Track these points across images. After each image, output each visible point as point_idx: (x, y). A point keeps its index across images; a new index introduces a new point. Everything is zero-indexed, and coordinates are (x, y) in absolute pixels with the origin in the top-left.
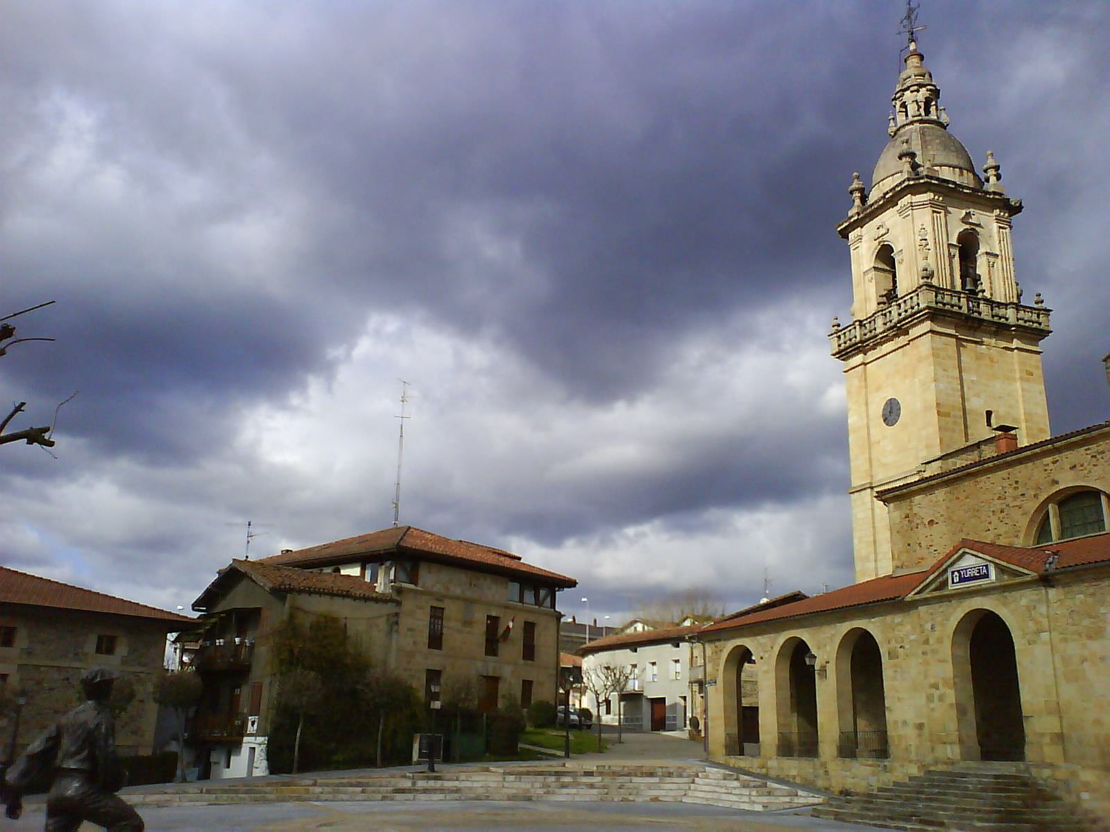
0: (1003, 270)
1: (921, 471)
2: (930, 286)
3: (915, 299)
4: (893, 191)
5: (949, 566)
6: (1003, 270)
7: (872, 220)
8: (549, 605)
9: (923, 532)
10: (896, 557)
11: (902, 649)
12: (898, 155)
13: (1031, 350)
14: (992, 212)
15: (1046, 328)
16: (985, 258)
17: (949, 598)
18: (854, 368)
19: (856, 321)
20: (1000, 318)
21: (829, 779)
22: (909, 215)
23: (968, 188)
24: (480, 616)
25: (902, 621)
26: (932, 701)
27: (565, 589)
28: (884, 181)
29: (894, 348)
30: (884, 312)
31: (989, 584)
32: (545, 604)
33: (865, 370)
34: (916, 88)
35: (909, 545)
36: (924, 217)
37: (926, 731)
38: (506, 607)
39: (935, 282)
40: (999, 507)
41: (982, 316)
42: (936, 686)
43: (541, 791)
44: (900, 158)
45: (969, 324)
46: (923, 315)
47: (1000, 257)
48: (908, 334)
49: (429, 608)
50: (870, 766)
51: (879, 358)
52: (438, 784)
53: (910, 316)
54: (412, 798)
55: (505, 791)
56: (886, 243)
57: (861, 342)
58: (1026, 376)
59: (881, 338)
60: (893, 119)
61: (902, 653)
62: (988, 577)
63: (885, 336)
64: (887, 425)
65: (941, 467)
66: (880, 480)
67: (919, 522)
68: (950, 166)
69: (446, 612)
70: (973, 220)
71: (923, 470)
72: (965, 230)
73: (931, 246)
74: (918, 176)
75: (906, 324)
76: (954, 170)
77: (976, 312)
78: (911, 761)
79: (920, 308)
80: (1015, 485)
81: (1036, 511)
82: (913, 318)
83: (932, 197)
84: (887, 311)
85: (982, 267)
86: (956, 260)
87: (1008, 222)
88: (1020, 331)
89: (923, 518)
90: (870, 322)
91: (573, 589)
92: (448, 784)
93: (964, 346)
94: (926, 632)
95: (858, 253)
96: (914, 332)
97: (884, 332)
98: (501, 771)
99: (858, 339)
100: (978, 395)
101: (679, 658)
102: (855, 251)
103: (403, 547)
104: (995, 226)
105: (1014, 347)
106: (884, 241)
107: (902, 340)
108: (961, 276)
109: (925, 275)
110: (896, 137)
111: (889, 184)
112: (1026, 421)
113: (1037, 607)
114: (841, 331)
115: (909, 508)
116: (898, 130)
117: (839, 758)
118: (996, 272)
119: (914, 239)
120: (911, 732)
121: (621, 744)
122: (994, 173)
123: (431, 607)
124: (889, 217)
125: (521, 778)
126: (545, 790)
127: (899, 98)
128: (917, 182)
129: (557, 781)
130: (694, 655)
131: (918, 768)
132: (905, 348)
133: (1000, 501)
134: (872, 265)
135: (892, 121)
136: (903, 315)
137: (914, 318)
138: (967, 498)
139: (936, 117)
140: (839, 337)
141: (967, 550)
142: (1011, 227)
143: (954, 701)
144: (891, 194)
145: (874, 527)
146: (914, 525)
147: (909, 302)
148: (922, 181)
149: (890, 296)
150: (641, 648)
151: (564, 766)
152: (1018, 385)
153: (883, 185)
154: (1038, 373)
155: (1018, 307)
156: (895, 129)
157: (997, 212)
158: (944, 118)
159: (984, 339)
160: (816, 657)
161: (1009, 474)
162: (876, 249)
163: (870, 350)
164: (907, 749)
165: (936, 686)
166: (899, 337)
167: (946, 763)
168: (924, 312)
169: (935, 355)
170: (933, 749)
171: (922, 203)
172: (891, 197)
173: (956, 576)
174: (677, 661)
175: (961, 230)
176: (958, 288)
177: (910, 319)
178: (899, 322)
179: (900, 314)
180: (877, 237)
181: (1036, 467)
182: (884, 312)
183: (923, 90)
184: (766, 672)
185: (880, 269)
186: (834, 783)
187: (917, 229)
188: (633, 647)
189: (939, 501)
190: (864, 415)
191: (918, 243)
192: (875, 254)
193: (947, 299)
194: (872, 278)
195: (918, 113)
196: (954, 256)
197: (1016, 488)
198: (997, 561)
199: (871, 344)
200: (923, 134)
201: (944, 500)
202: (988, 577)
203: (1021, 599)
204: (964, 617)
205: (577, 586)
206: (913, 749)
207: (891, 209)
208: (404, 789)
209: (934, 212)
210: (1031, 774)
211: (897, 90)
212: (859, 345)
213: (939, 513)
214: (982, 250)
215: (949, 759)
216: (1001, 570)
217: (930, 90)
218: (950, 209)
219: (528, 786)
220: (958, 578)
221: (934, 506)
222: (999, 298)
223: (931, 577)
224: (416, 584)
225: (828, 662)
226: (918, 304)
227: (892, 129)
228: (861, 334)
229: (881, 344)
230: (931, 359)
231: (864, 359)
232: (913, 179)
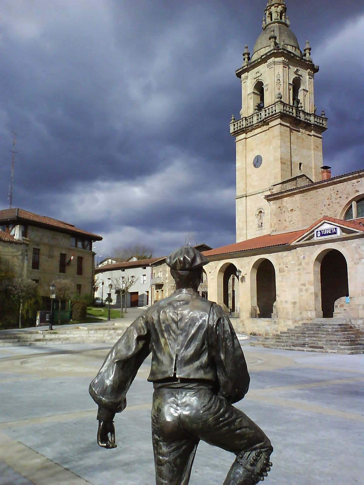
0: (309, 98)
1: (271, 189)
2: (281, 102)
3: (274, 108)
4: (266, 55)
5: (316, 229)
6: (309, 98)
7: (253, 69)
8: (89, 249)
9: (287, 215)
10: (273, 226)
11: (287, 268)
12: (269, 37)
13: (319, 137)
14: (307, 70)
15: (325, 127)
16: (303, 91)
17: (313, 244)
18: (241, 140)
19: (244, 118)
20: (308, 120)
21: (245, 328)
22: (272, 67)
23: (299, 57)
24: (57, 254)
25: (287, 255)
26: (302, 291)
27: (96, 241)
28: (261, 50)
29: (261, 131)
30: (258, 114)
31: (337, 237)
32: (87, 248)
33: (246, 141)
34: (277, 5)
35: (280, 221)
36: (279, 69)
37: (298, 305)
38: (69, 249)
39: (282, 100)
40: (327, 203)
41: (301, 119)
42: (304, 285)
43: (109, 338)
44: (270, 39)
45: (296, 122)
46: (276, 116)
47: (309, 92)
48: (269, 125)
49: (32, 249)
50: (267, 321)
51: (253, 136)
52: (56, 336)
53: (271, 116)
54: (45, 344)
55: (90, 338)
56: (260, 81)
57: (246, 128)
58: (316, 148)
59: (255, 126)
60: (265, 20)
61: (287, 270)
62: (336, 234)
63: (257, 126)
64: (255, 167)
65: (281, 187)
66: (250, 193)
67: (285, 210)
68: (291, 46)
69: (41, 251)
70: (299, 73)
71: (272, 188)
72: (296, 77)
73: (282, 83)
74: (278, 48)
75: (268, 120)
76: (292, 48)
77: (299, 116)
78: (289, 319)
79: (276, 112)
80: (337, 193)
81: (346, 205)
82: (272, 117)
83: (284, 59)
84: (259, 113)
85: (301, 96)
86: (291, 91)
87: (312, 76)
88: (315, 127)
89: (287, 208)
90: (250, 118)
91: (100, 241)
92: (61, 336)
93: (292, 132)
94: (300, 260)
95: (245, 85)
96: (271, 124)
97: (257, 123)
98: (86, 328)
99: (244, 126)
100: (296, 155)
101: (135, 275)
102: (244, 84)
103: (20, 217)
104: (308, 77)
105: (312, 134)
106: (259, 80)
107: (265, 128)
108: (293, 99)
109: (279, 96)
110: (266, 29)
111: (263, 52)
112: (315, 168)
113: (360, 247)
114: (236, 122)
115: (281, 203)
116: (268, 25)
117: (251, 318)
118: (306, 99)
119: (275, 79)
120: (289, 306)
121: (126, 314)
122: (308, 51)
123: (34, 248)
124: (262, 68)
125: (97, 332)
126: (111, 337)
127: (268, 10)
128: (278, 51)
129: (115, 332)
130: (153, 272)
131: (292, 322)
132: (266, 131)
133: (328, 200)
134: (252, 91)
135: (264, 21)
136: (267, 115)
137: (273, 117)
138: (311, 199)
139: (284, 21)
140: (234, 125)
141: (326, 221)
142: (313, 79)
143: (314, 292)
144: (264, 56)
145: (246, 215)
146: (283, 211)
147: (271, 110)
148: (280, 51)
149: (260, 107)
150: (127, 270)
151: (114, 325)
152: (312, 152)
153: (260, 52)
154: (321, 147)
155: (315, 116)
156: (265, 25)
157: (309, 70)
158: (288, 22)
159: (300, 129)
160: (241, 272)
161: (334, 188)
162: (255, 83)
163: (249, 132)
164: (287, 313)
165: (304, 285)
166: (264, 126)
167: (307, 319)
168: (277, 115)
169: (281, 135)
170: (301, 313)
171: (279, 62)
172: (265, 58)
173: (319, 233)
174: (144, 275)
175: (294, 77)
176: (291, 104)
177: (271, 118)
178: (265, 119)
179: (266, 115)
180: (255, 77)
181: (348, 184)
182: (258, 114)
183: (280, 7)
184: (212, 279)
185: (256, 93)
186: (247, 329)
187: (276, 75)
188: (123, 269)
189: (296, 200)
190: (244, 163)
191: (276, 82)
192: (254, 85)
193: (288, 109)
194: (252, 98)
195: (277, 18)
196: (291, 89)
197: (337, 194)
198: (342, 226)
199: (250, 129)
200: (280, 29)
201: (299, 200)
202: (336, 234)
203: (352, 244)
204: (321, 252)
205: (103, 240)
206: (290, 313)
207: (263, 64)
208: (40, 339)
209: (284, 67)
210: (352, 323)
211: (267, 5)
212: (244, 129)
213: (297, 206)
214: (302, 88)
215: (309, 317)
216: (343, 230)
217: (283, 7)
218: (290, 66)
219: (102, 335)
220: (320, 234)
221: (294, 203)
222: (307, 111)
223: (306, 234)
224: (26, 237)
225: (246, 274)
226: (275, 111)
227: (264, 25)
228: (245, 124)
229: (255, 129)
230: (279, 137)
231: (246, 136)
232: (276, 50)
